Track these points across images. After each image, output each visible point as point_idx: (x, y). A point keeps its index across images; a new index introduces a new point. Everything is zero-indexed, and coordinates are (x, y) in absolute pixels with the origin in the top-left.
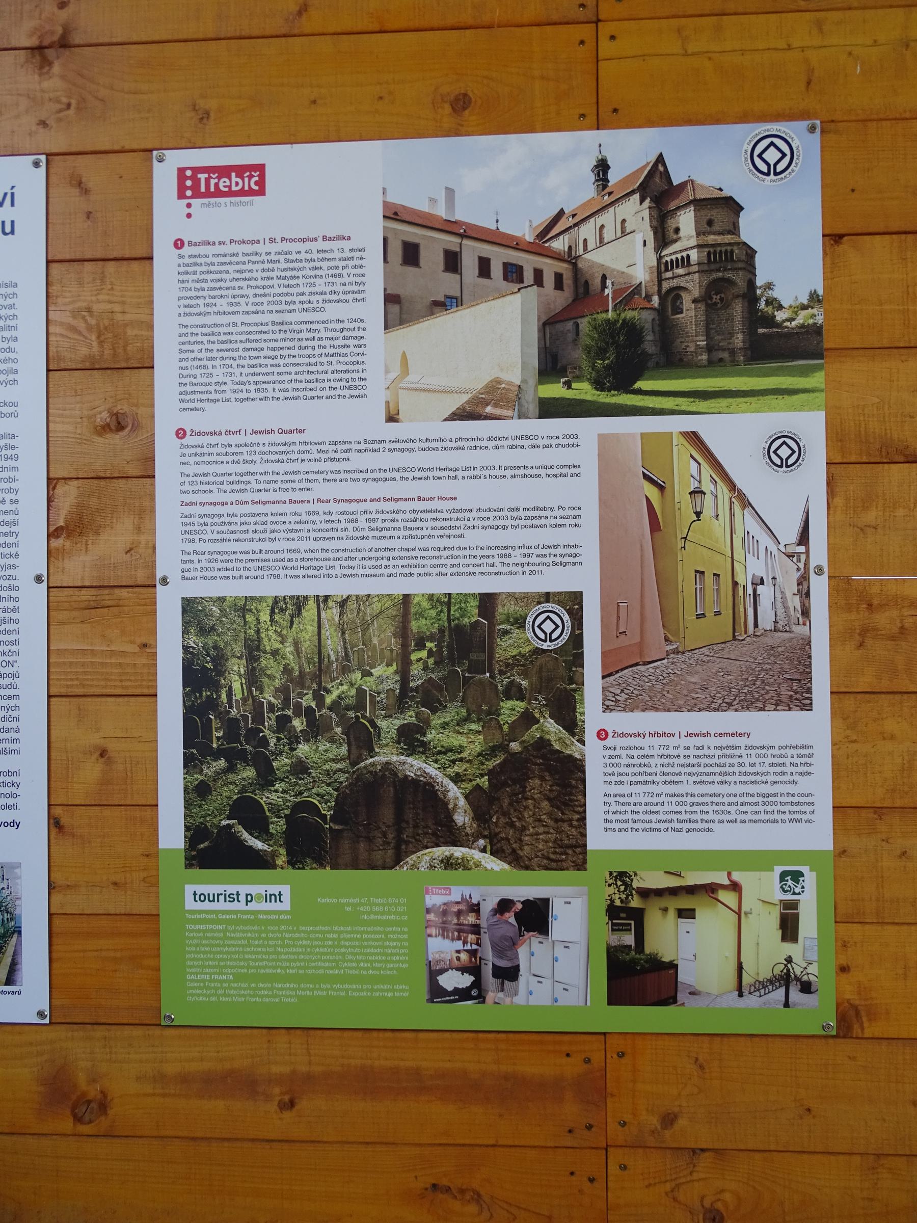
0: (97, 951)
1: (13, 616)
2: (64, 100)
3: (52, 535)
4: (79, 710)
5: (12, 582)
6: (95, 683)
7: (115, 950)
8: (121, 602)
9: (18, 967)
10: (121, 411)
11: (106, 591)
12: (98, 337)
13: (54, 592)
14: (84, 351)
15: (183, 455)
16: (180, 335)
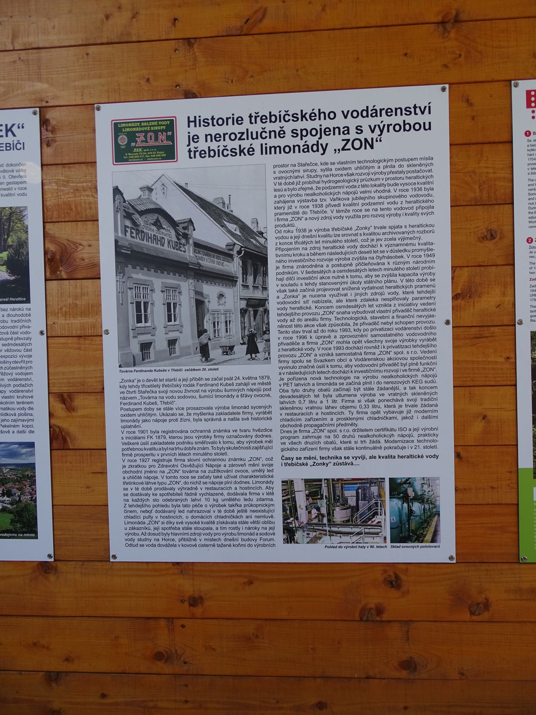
0: (481, 524)
1: (433, 343)
2: (458, 52)
3: (455, 297)
4: (470, 393)
5: (432, 325)
6: (480, 379)
7: (491, 523)
8: (494, 335)
9: (438, 533)
10: (493, 229)
11: (486, 329)
12: (480, 187)
13: (51, 340)
14: (472, 195)
15: (531, 252)
16: (529, 185)
